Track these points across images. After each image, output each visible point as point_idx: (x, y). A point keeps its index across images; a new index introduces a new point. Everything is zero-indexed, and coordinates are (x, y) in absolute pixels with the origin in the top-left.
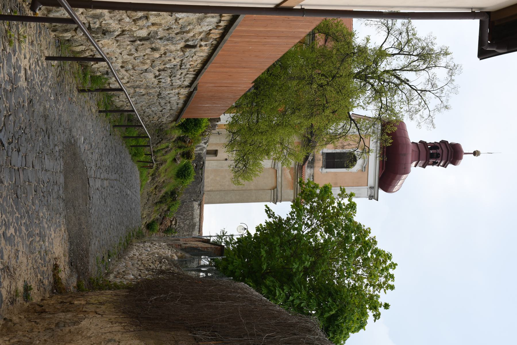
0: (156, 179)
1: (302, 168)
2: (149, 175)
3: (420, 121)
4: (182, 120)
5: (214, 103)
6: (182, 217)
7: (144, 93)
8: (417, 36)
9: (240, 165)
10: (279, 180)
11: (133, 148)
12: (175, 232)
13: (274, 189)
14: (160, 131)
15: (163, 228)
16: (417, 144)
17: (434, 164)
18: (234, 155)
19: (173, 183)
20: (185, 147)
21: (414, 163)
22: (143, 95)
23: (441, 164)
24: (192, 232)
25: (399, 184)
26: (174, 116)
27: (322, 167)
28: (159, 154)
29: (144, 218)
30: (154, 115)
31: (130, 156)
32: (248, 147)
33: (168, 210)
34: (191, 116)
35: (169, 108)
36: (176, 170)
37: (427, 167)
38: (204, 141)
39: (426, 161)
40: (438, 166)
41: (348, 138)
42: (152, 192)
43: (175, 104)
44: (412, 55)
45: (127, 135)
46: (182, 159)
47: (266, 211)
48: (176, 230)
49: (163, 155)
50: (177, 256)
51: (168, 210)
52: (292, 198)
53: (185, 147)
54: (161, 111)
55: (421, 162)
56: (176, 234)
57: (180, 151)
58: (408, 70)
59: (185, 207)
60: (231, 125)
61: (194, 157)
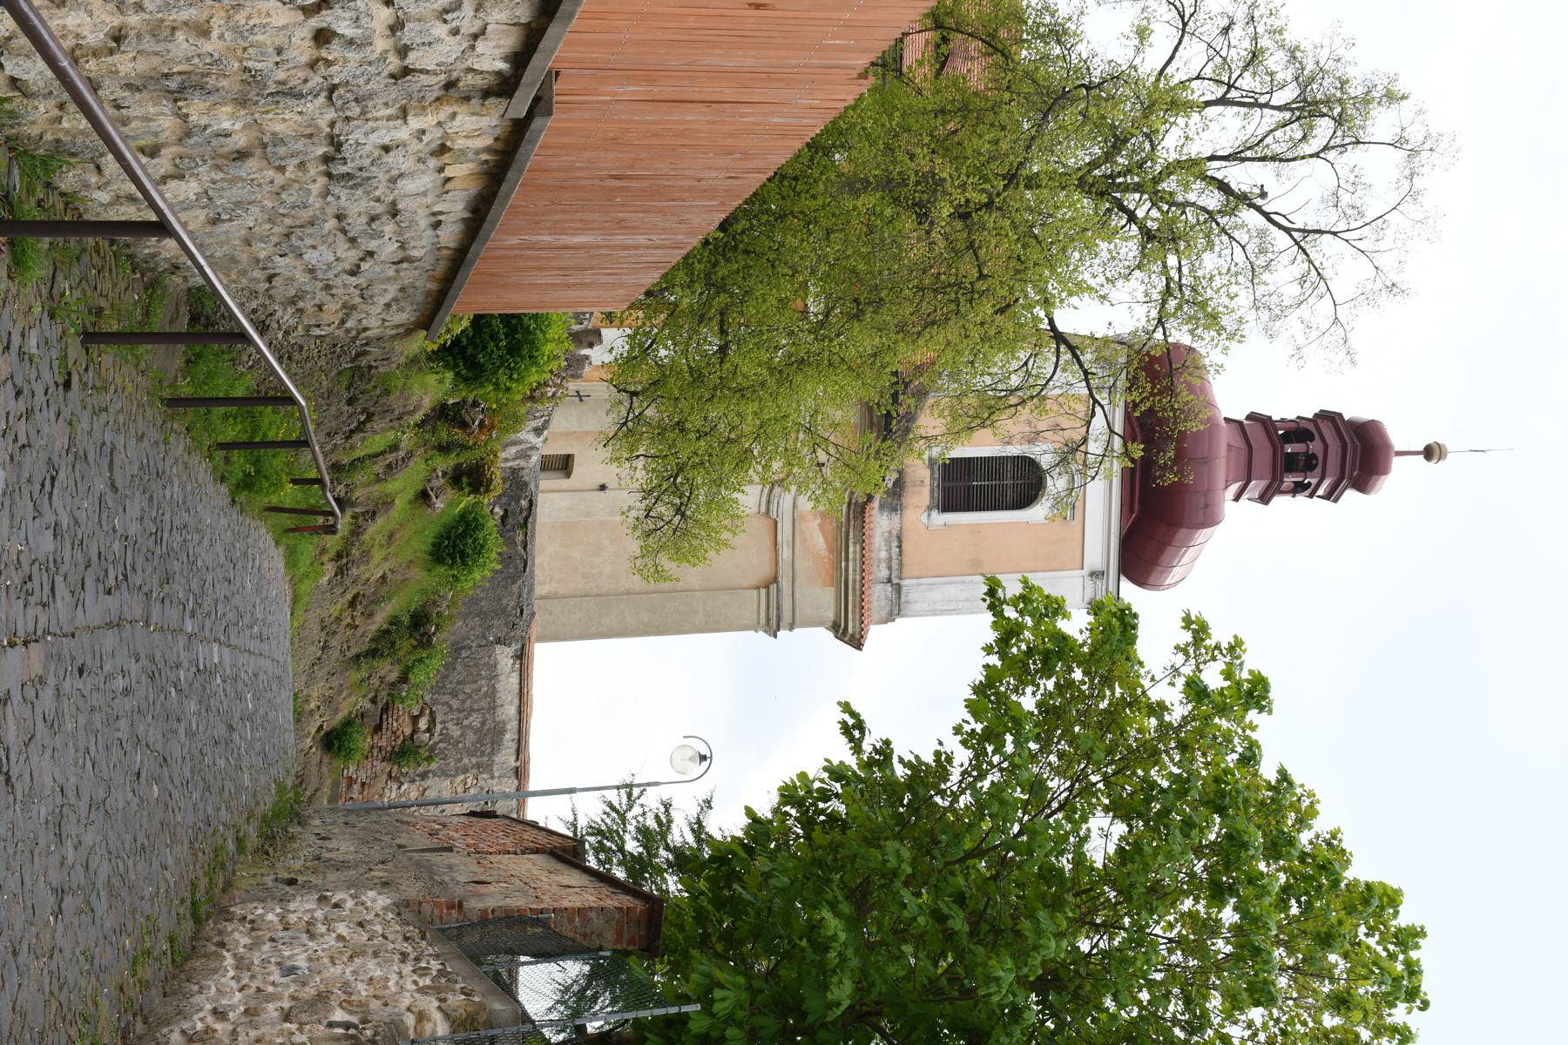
0: (354, 571)
1: (863, 512)
2: (325, 558)
3: (1301, 341)
4: (455, 322)
5: (621, 225)
6: (455, 703)
7: (240, 141)
8: (1286, 35)
9: (663, 509)
10: (785, 553)
11: (235, 455)
12: (429, 759)
13: (767, 587)
14: (356, 376)
15: (383, 743)
16: (1240, 423)
17: (1298, 488)
18: (640, 474)
19: (418, 583)
20: (464, 447)
21: (1234, 488)
22: (241, 155)
23: (1321, 492)
24: (493, 753)
25: (1185, 560)
26: (419, 298)
27: (930, 508)
28: (359, 477)
29: (311, 712)
30: (321, 296)
31: (224, 489)
32: (687, 443)
33: (404, 679)
34: (496, 302)
35: (389, 249)
36: (430, 535)
37: (1278, 501)
38: (534, 424)
39: (1274, 479)
40: (1311, 496)
41: (1049, 404)
42: (338, 620)
43: (424, 222)
44: (1266, 105)
45: (185, 390)
46: (450, 493)
47: (846, 730)
48: (432, 749)
49: (378, 480)
50: (446, 1015)
51: (404, 679)
52: (830, 615)
53: (464, 447)
54: (354, 272)
55: (1256, 487)
56: (434, 766)
57: (444, 463)
58: (1253, 159)
59: (466, 666)
60: (628, 363)
61: (497, 480)
